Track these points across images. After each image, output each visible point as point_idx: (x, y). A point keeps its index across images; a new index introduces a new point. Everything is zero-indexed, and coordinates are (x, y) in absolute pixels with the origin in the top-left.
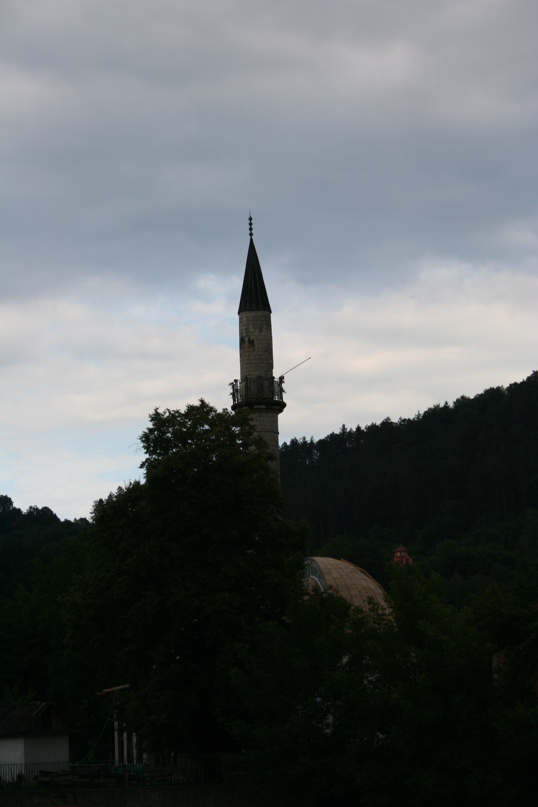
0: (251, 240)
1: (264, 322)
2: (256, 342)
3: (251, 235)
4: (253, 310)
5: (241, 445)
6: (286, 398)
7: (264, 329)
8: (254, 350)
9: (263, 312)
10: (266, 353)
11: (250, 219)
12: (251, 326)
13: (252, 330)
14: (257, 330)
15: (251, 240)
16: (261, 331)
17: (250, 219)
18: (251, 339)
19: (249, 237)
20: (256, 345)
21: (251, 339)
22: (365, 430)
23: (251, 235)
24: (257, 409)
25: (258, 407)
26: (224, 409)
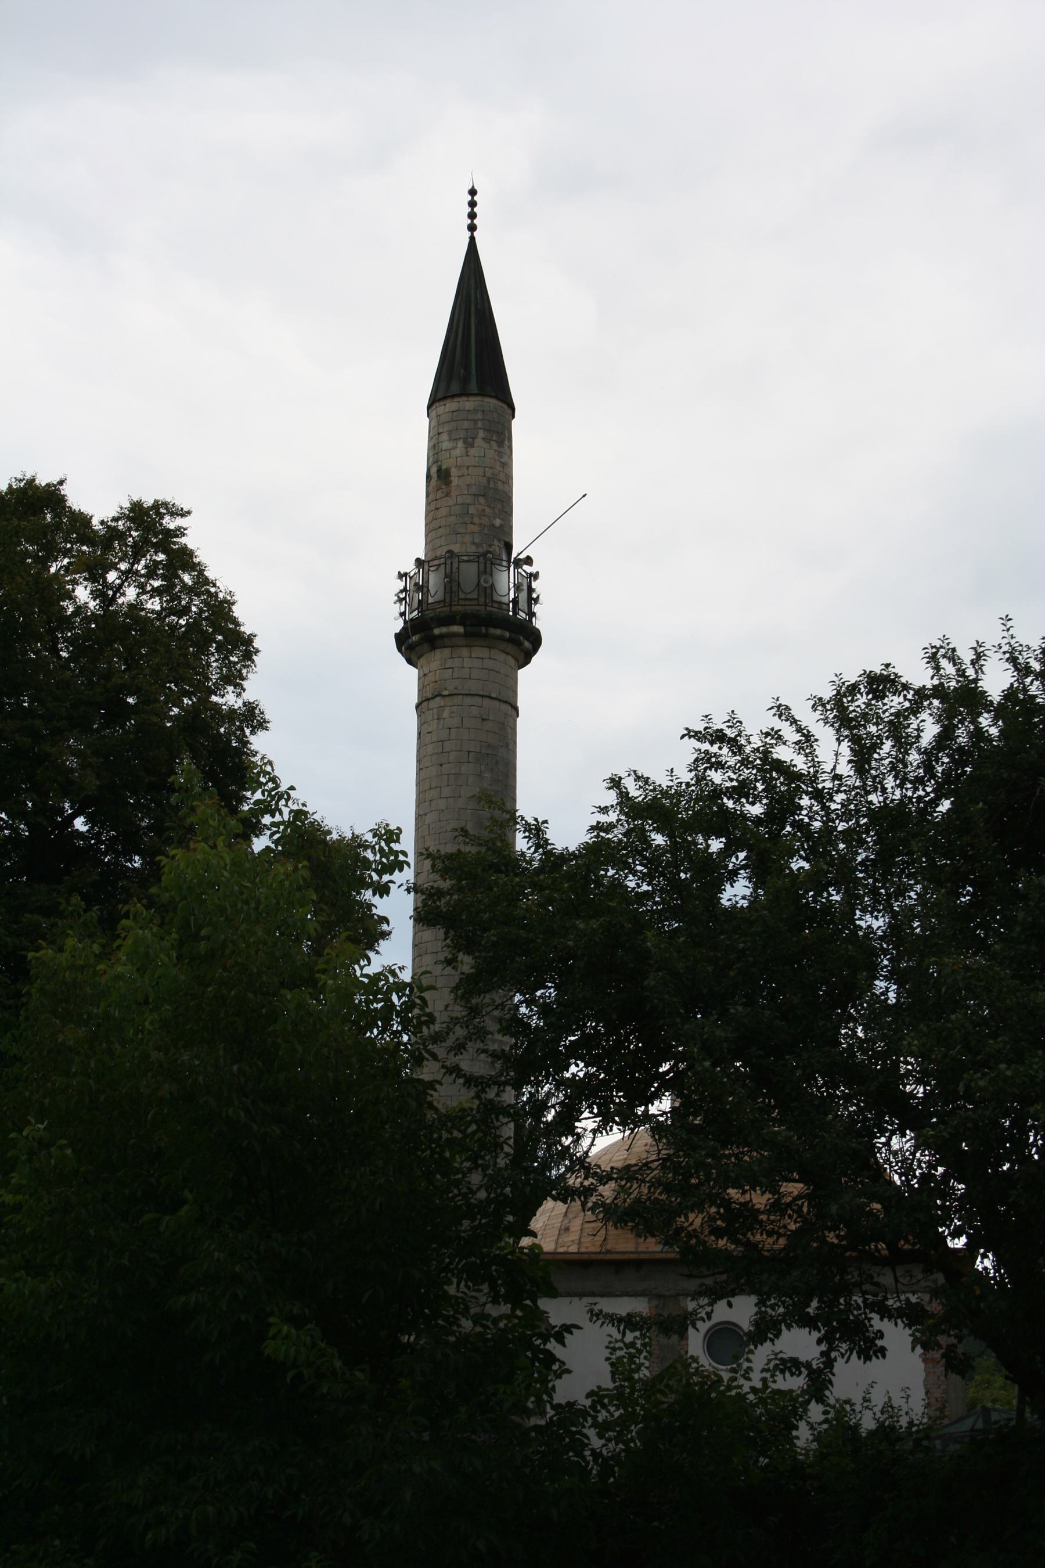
0: (472, 239)
1: (480, 424)
2: (454, 472)
3: (472, 228)
4: (453, 396)
5: (149, 828)
6: (405, 680)
7: (479, 442)
8: (447, 495)
9: (479, 398)
10: (482, 500)
11: (473, 192)
12: (445, 437)
13: (446, 445)
14: (460, 444)
15: (472, 239)
16: (469, 444)
17: (473, 192)
18: (444, 467)
19: (469, 234)
20: (455, 481)
21: (444, 467)
22: (752, 1329)
23: (472, 228)
24: (442, 636)
25: (444, 630)
26: (398, 828)
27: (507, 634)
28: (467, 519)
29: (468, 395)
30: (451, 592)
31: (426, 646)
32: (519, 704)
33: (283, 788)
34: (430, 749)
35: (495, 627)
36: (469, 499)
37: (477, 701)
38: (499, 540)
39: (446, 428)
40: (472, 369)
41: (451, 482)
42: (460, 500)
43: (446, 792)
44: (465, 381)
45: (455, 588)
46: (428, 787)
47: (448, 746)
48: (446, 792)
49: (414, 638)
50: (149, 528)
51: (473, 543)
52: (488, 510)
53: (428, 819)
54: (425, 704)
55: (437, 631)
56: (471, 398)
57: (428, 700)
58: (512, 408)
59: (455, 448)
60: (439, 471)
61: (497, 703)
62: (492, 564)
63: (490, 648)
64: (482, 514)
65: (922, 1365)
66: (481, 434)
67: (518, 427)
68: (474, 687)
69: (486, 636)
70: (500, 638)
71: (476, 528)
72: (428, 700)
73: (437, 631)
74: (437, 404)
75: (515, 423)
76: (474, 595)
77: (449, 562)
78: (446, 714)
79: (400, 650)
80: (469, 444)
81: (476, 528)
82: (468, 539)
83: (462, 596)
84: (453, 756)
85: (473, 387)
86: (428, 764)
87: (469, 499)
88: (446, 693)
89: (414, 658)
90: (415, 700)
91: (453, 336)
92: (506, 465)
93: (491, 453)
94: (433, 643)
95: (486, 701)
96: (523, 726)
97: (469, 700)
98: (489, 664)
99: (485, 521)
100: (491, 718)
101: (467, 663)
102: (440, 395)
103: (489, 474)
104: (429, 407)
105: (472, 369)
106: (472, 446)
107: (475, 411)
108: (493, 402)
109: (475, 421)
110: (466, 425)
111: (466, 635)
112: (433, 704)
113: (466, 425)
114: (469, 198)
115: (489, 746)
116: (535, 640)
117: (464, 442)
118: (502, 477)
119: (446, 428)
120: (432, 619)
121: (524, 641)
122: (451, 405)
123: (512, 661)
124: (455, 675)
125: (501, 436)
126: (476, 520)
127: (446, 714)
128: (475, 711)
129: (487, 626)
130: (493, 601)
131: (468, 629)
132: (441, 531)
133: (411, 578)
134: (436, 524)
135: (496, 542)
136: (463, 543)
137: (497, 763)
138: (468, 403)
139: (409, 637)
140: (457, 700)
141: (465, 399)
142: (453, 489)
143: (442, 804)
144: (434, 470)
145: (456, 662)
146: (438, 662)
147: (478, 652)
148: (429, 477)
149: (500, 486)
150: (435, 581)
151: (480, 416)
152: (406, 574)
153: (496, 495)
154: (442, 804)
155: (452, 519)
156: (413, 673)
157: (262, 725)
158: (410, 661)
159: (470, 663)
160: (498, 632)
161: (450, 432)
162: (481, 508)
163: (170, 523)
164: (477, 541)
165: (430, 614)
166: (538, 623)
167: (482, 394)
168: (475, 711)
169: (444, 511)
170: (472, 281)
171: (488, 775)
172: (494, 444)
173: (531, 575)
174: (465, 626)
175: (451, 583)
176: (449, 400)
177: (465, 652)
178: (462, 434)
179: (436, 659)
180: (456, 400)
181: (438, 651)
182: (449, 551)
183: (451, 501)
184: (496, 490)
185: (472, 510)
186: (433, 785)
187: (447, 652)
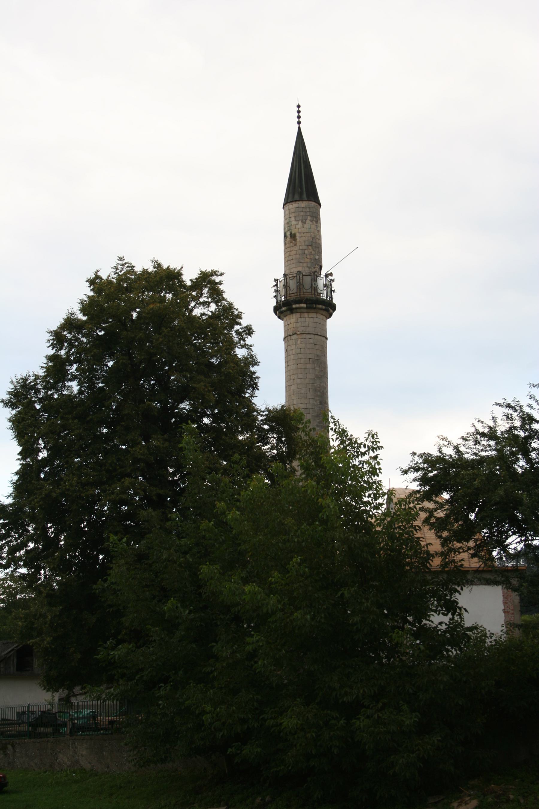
0: (299, 128)
1: (308, 214)
2: (298, 235)
3: (299, 123)
4: (296, 201)
7: (308, 221)
8: (295, 245)
9: (307, 202)
10: (310, 247)
11: (299, 106)
12: (293, 219)
13: (294, 223)
14: (300, 222)
15: (299, 128)
16: (304, 223)
17: (299, 106)
18: (293, 233)
19: (298, 125)
20: (298, 239)
21: (293, 233)
23: (299, 123)
24: (296, 308)
25: (297, 306)
27: (324, 307)
28: (305, 256)
29: (303, 200)
30: (300, 288)
31: (289, 312)
32: (328, 336)
33: (336, 420)
34: (292, 357)
35: (319, 304)
36: (305, 247)
37: (312, 336)
38: (318, 265)
39: (293, 215)
40: (302, 186)
41: (296, 239)
42: (301, 247)
43: (300, 376)
44: (301, 194)
45: (302, 287)
46: (291, 374)
47: (300, 356)
48: (300, 376)
49: (284, 309)
50: (207, 281)
51: (308, 267)
52: (313, 252)
53: (293, 387)
54: (289, 337)
55: (294, 306)
56: (304, 202)
57: (290, 335)
58: (320, 205)
59: (298, 224)
60: (291, 234)
61: (320, 337)
62: (317, 276)
63: (317, 313)
64: (310, 254)
65: (503, 614)
66: (309, 218)
67: (323, 211)
68: (311, 330)
69: (315, 308)
70: (321, 309)
71: (308, 260)
72: (290, 335)
73: (294, 306)
74: (289, 204)
75: (321, 210)
76: (310, 291)
77: (298, 277)
78: (299, 342)
79: (276, 314)
80: (304, 223)
81: (308, 260)
82: (305, 265)
83: (305, 291)
84: (303, 360)
85: (305, 196)
86: (292, 364)
87: (305, 247)
88: (299, 333)
89: (282, 316)
90: (282, 336)
91: (294, 173)
92: (319, 231)
93: (313, 226)
94: (292, 311)
95: (316, 336)
96: (330, 344)
97: (308, 336)
98: (316, 320)
99: (312, 257)
100: (318, 343)
101: (307, 320)
102: (290, 200)
103: (313, 236)
104: (285, 204)
105: (302, 186)
106: (305, 223)
107: (306, 208)
108: (313, 203)
109: (306, 212)
110: (302, 214)
111: (307, 308)
112: (292, 337)
113: (302, 214)
114: (297, 109)
115: (318, 356)
116: (333, 307)
117: (302, 222)
118: (318, 237)
119: (293, 215)
120: (292, 301)
121: (329, 308)
122: (295, 205)
123: (325, 318)
124: (303, 325)
125: (316, 218)
126: (308, 257)
127: (299, 342)
128: (311, 341)
129: (316, 304)
130: (318, 293)
131: (308, 305)
132: (293, 261)
133: (280, 282)
134: (290, 258)
135: (317, 266)
136: (303, 267)
137: (321, 363)
138: (303, 204)
139: (281, 308)
140: (304, 336)
141: (301, 202)
142: (298, 243)
143: (299, 381)
144: (288, 234)
145: (302, 320)
146: (294, 319)
147: (311, 315)
148: (285, 236)
149: (317, 241)
150: (293, 284)
151: (308, 210)
152: (277, 280)
153: (315, 245)
154: (299, 381)
155: (298, 256)
156: (281, 323)
157: (256, 364)
158: (279, 317)
159: (308, 319)
160: (320, 306)
161: (295, 217)
162: (310, 251)
163: (217, 279)
164: (309, 266)
165: (292, 298)
166: (334, 301)
167: (309, 200)
168: (311, 341)
169: (294, 252)
170: (301, 148)
171: (318, 369)
172: (314, 222)
173: (331, 280)
174: (306, 304)
175: (300, 285)
176: (294, 203)
177: (306, 315)
178: (301, 218)
179: (293, 318)
180: (297, 202)
181: (294, 315)
182: (299, 271)
183: (297, 248)
184: (316, 243)
185: (306, 252)
186: (295, 373)
187: (298, 315)
